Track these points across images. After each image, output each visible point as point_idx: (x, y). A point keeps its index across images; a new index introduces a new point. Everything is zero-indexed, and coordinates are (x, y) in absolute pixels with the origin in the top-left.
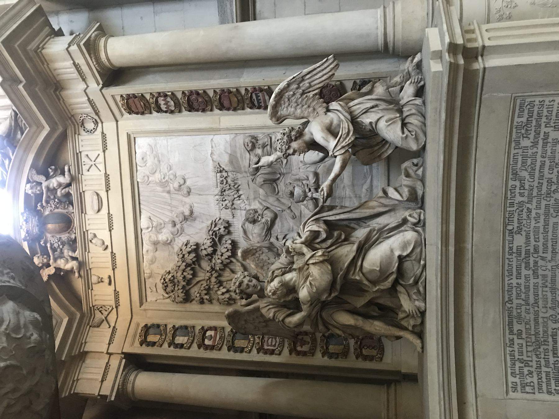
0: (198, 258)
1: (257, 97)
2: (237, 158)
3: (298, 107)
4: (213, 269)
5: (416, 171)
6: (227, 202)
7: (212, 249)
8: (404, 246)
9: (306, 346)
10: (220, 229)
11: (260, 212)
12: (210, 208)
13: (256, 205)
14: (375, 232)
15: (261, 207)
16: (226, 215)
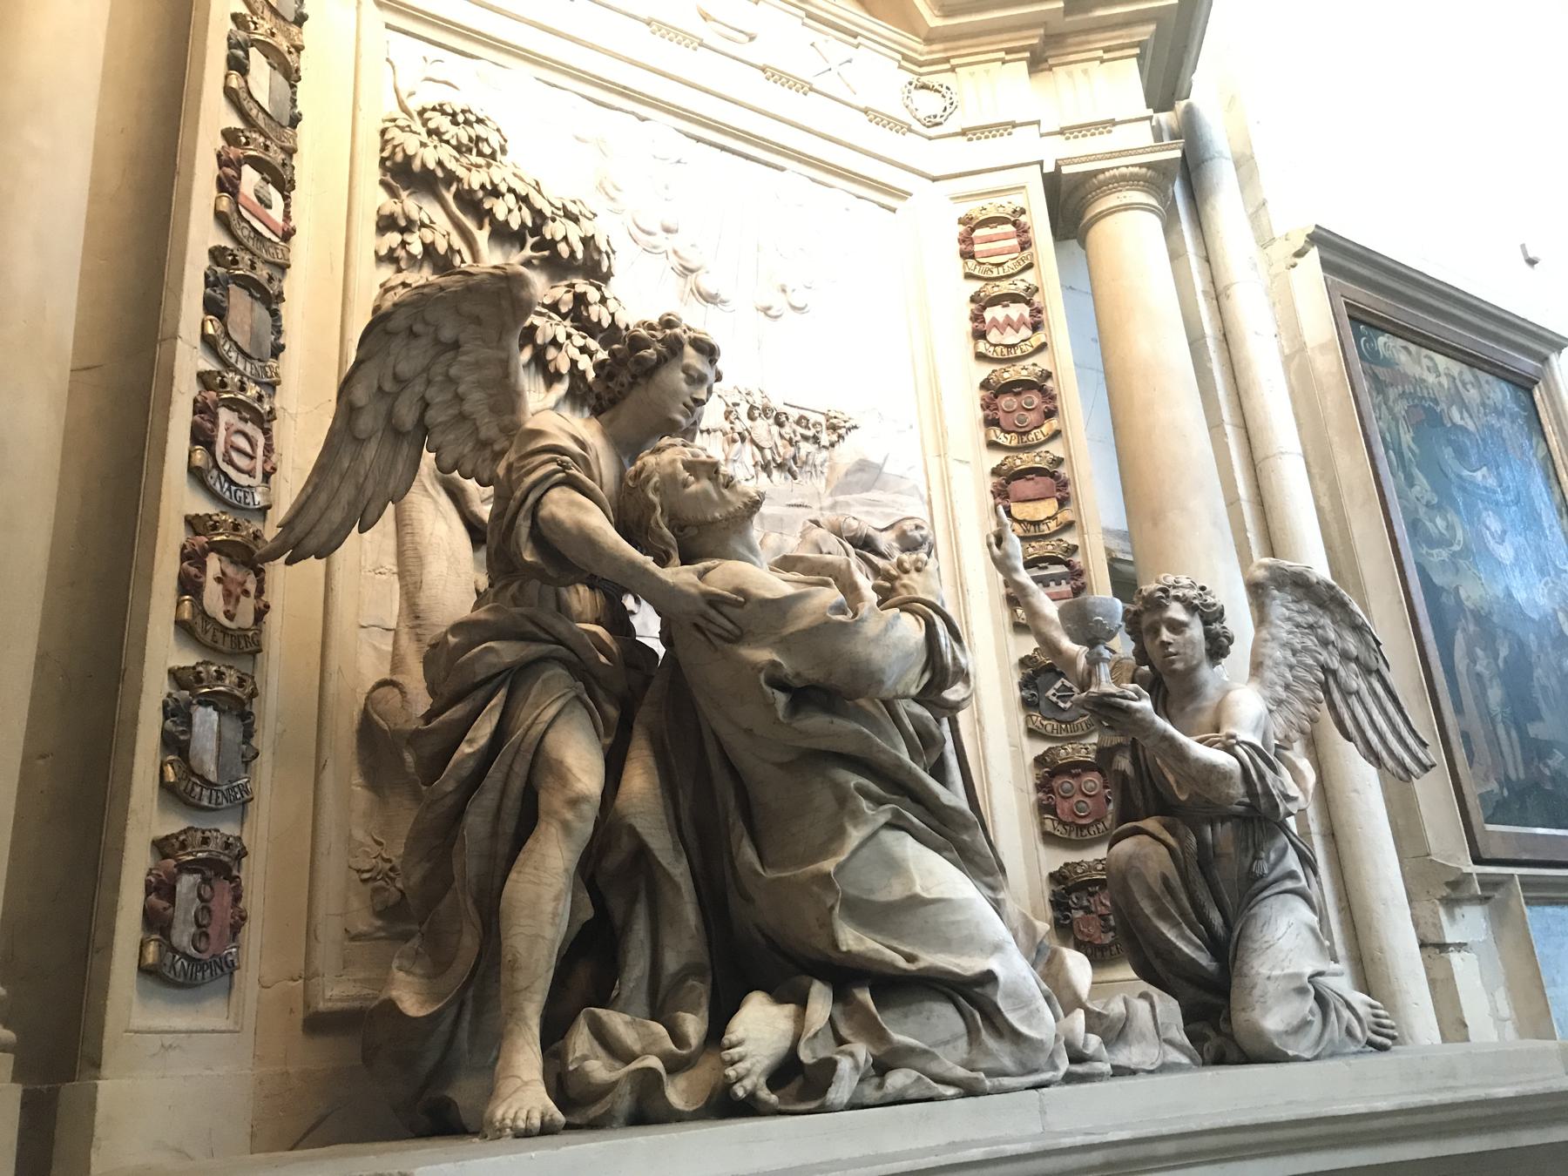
3: (1289, 654)
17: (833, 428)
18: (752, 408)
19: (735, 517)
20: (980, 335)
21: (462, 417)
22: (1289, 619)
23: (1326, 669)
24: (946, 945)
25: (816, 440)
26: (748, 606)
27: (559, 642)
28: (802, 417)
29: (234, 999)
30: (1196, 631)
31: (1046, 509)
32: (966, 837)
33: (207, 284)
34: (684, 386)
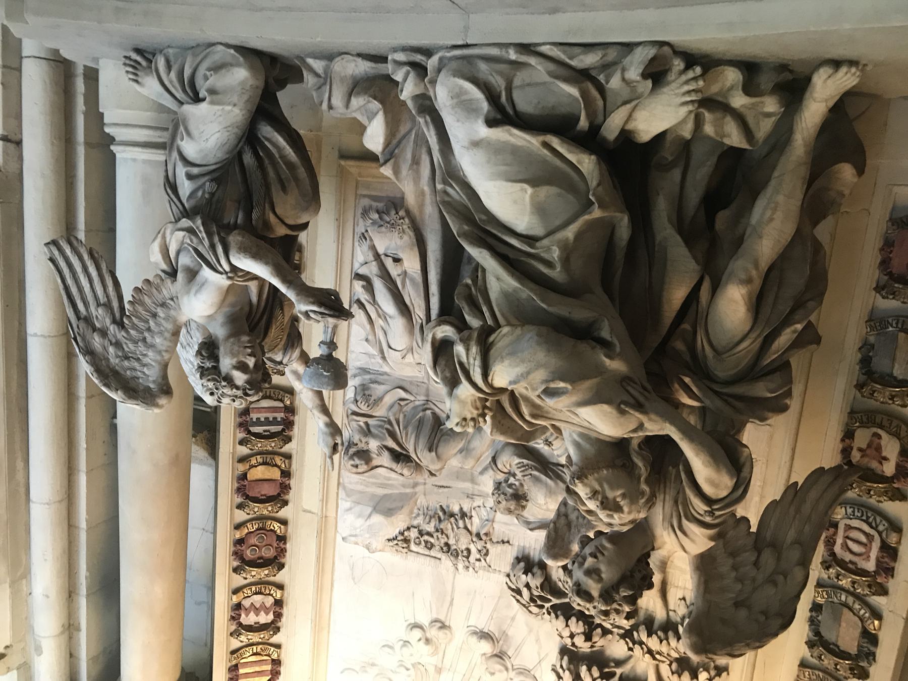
0: (598, 660)
1: (258, 423)
2: (385, 496)
3: (149, 339)
4: (627, 635)
5: (317, 75)
6: (473, 548)
7: (574, 619)
8: (466, 107)
9: (883, 443)
10: (527, 586)
11: (501, 477)
12: (483, 591)
13: (487, 483)
14: (449, 190)
15: (491, 472)
16: (502, 558)
17: (406, 541)
18: (468, 557)
19: (594, 469)
20: (279, 603)
21: (733, 554)
22: (144, 365)
23: (121, 325)
24: (515, 151)
25: (421, 533)
26: (619, 401)
27: (716, 393)
28: (430, 549)
29: (891, 206)
30: (226, 363)
31: (259, 472)
32: (466, 227)
33: (874, 655)
34: (603, 568)
